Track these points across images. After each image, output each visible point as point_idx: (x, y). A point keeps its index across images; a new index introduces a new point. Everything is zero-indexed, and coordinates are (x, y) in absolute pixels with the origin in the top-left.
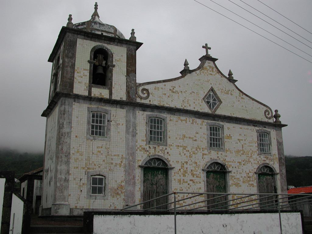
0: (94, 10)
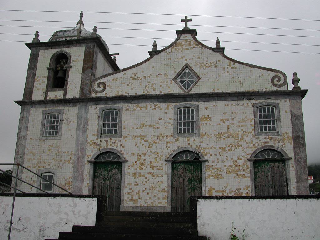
0: (79, 18)
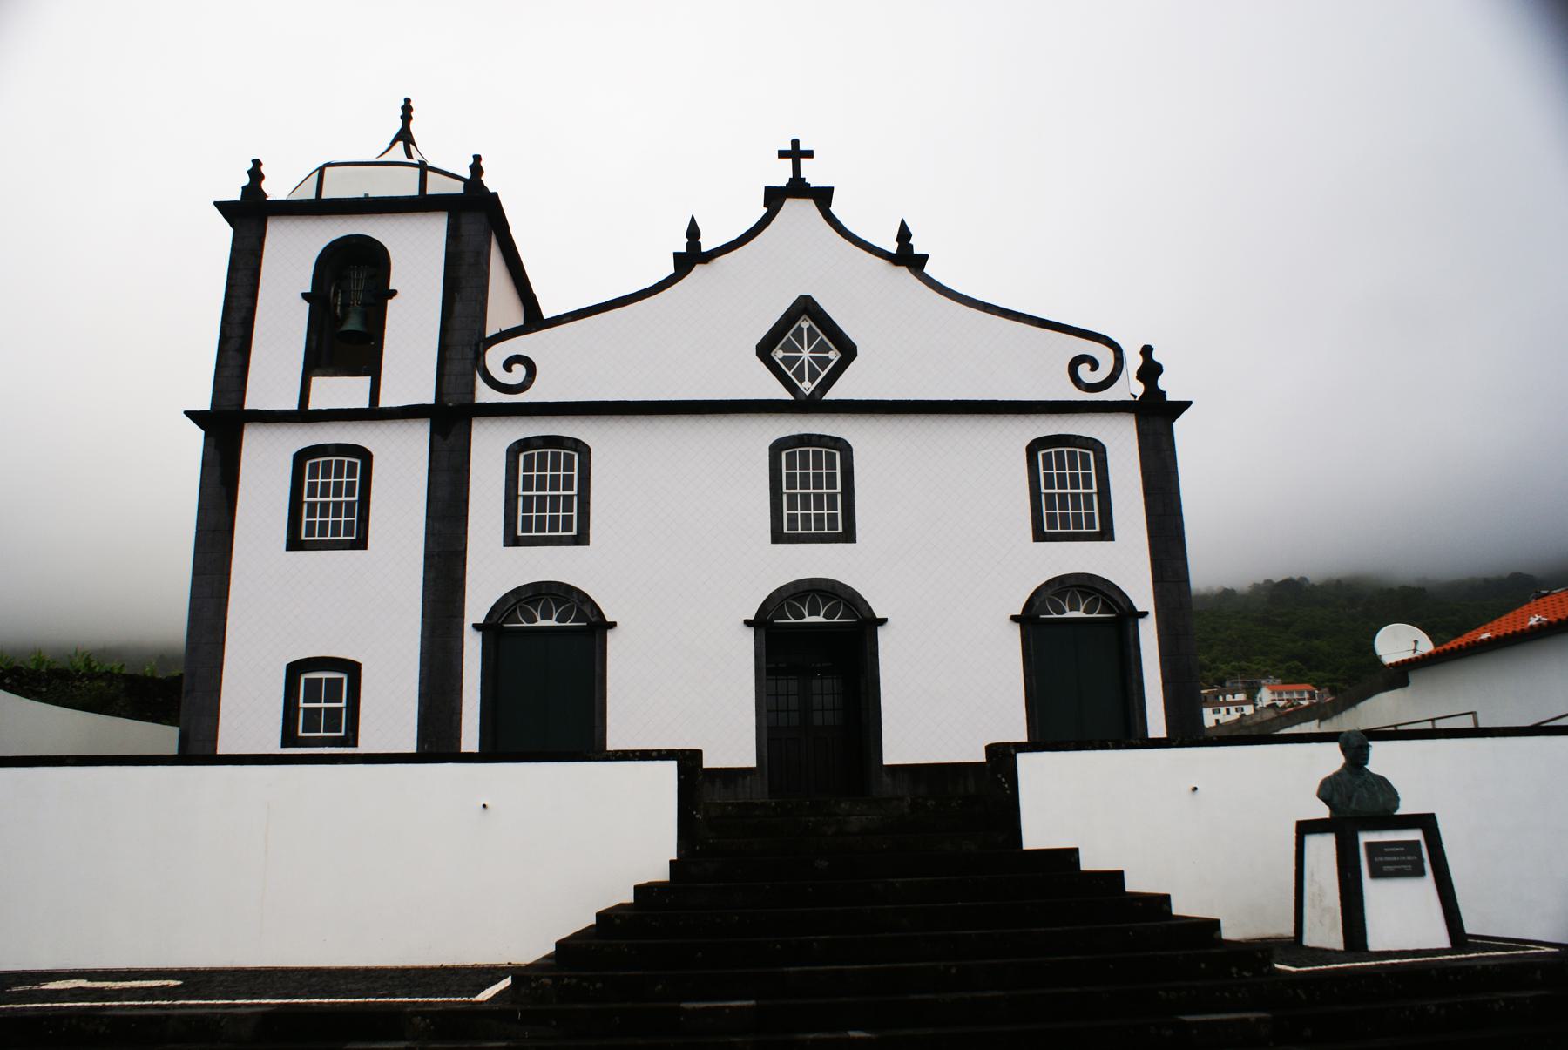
0: (399, 125)
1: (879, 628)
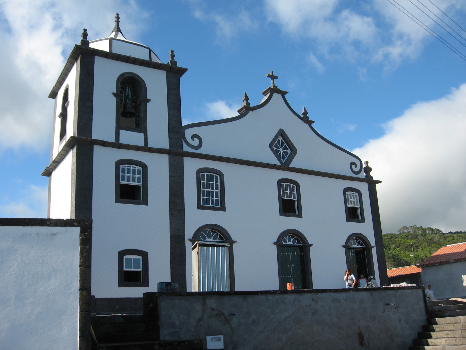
1: (233, 244)
